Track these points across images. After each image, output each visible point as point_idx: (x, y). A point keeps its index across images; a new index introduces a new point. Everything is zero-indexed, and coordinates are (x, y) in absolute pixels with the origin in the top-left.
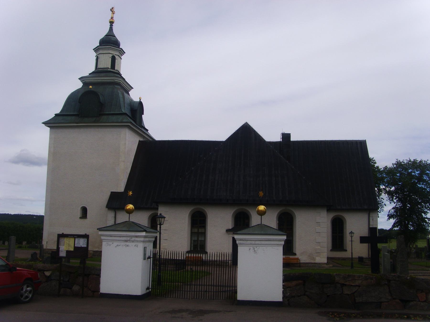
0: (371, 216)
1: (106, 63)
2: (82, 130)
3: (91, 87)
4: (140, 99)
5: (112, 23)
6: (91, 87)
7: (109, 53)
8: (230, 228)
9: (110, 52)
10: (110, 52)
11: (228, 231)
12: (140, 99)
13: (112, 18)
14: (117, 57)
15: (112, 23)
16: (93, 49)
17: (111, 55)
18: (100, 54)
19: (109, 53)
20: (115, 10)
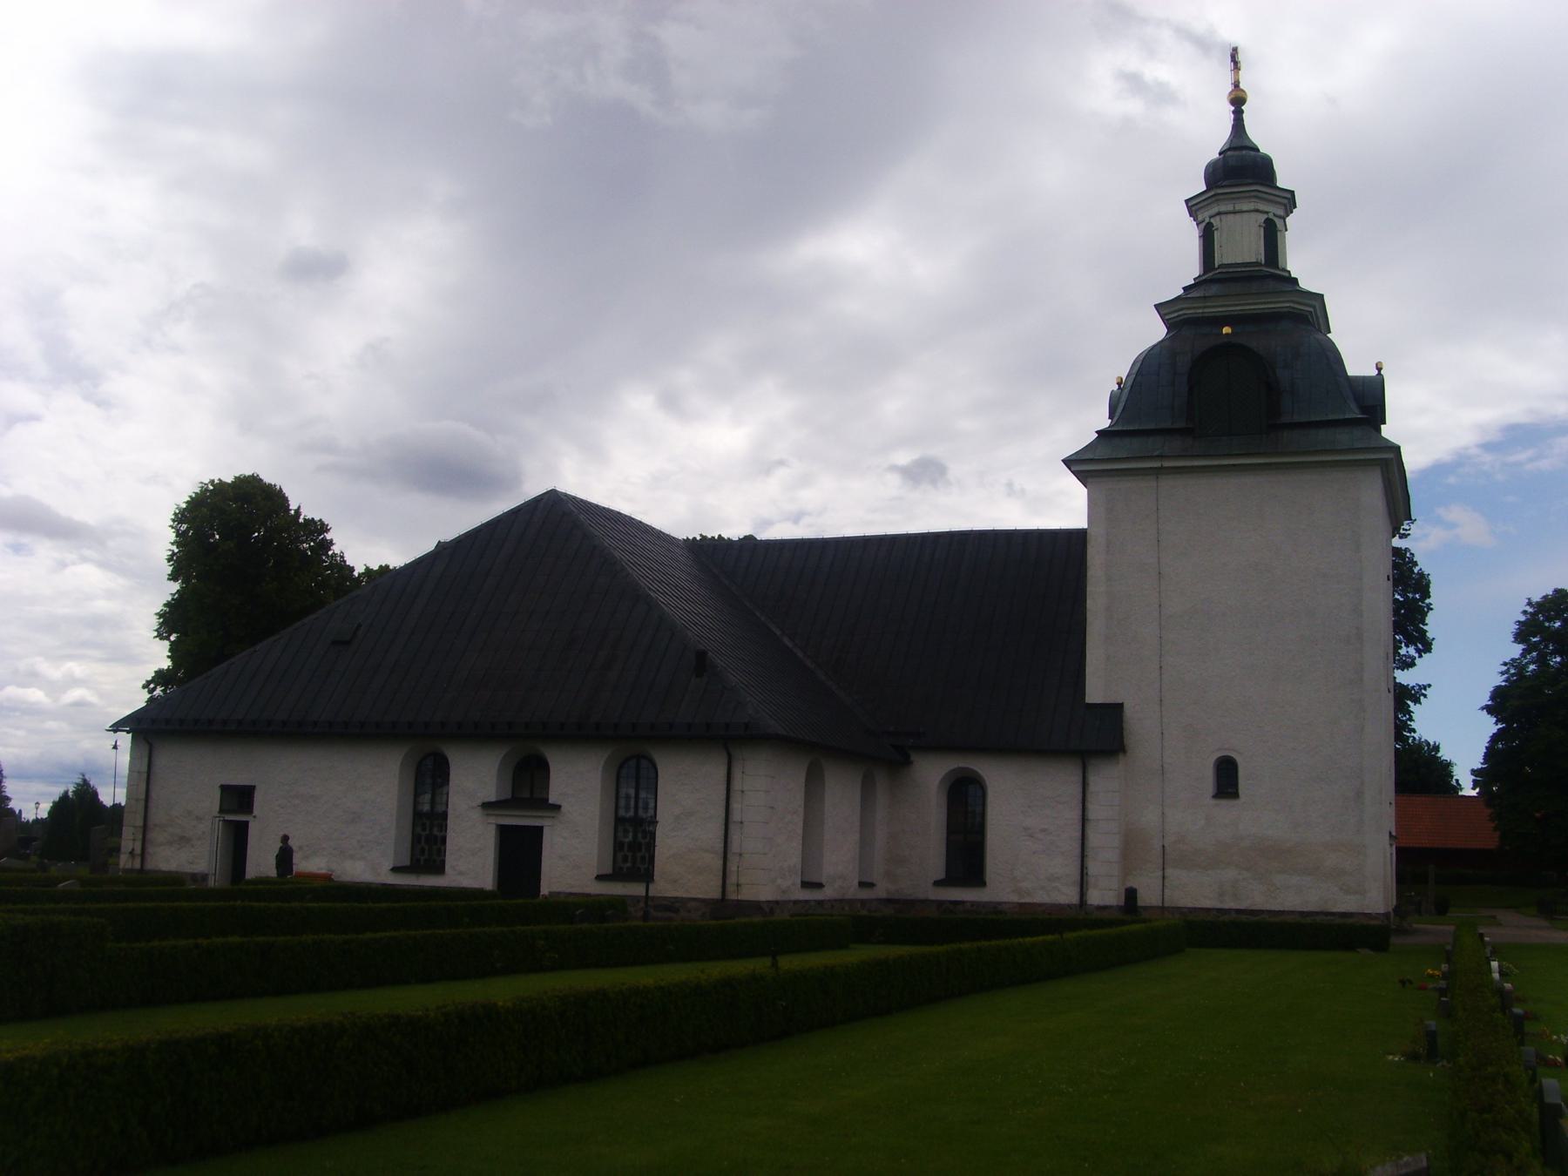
0: (1092, 779)
1: (1241, 246)
2: (1249, 480)
3: (1226, 330)
4: (1379, 369)
5: (1238, 101)
6: (1226, 330)
7: (1257, 211)
8: (493, 799)
9: (1262, 207)
10: (1262, 207)
11: (487, 806)
12: (1379, 369)
13: (1236, 85)
14: (1278, 222)
15: (1238, 101)
16: (1187, 201)
17: (1262, 218)
18: (1219, 213)
19: (1257, 211)
20: (1241, 57)
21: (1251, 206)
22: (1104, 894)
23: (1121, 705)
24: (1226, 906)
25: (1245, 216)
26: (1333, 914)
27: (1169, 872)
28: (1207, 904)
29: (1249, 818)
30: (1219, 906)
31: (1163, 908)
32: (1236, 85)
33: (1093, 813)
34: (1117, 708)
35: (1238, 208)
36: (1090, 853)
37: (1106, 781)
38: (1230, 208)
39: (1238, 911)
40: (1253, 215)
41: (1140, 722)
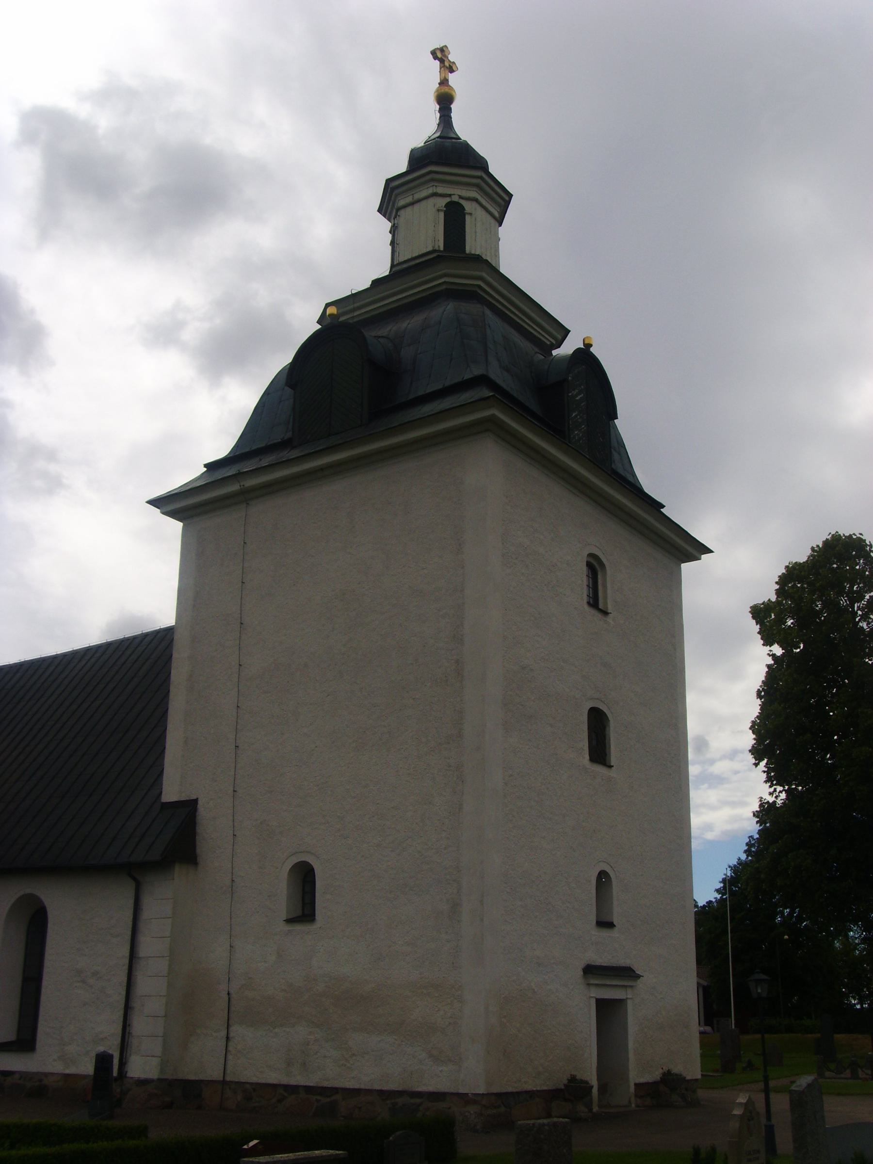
5: (445, 101)
9: (440, 190)
15: (445, 101)
17: (442, 202)
19: (435, 195)
21: (430, 191)
22: (142, 1066)
23: (195, 802)
24: (293, 1082)
25: (424, 203)
26: (419, 1095)
27: (237, 1030)
28: (273, 1077)
29: (332, 952)
30: (285, 1080)
31: (224, 1082)
32: (444, 82)
33: (143, 951)
34: (191, 805)
35: (418, 196)
36: (136, 1004)
37: (162, 899)
38: (409, 199)
39: (309, 1089)
40: (431, 201)
41: (213, 827)
